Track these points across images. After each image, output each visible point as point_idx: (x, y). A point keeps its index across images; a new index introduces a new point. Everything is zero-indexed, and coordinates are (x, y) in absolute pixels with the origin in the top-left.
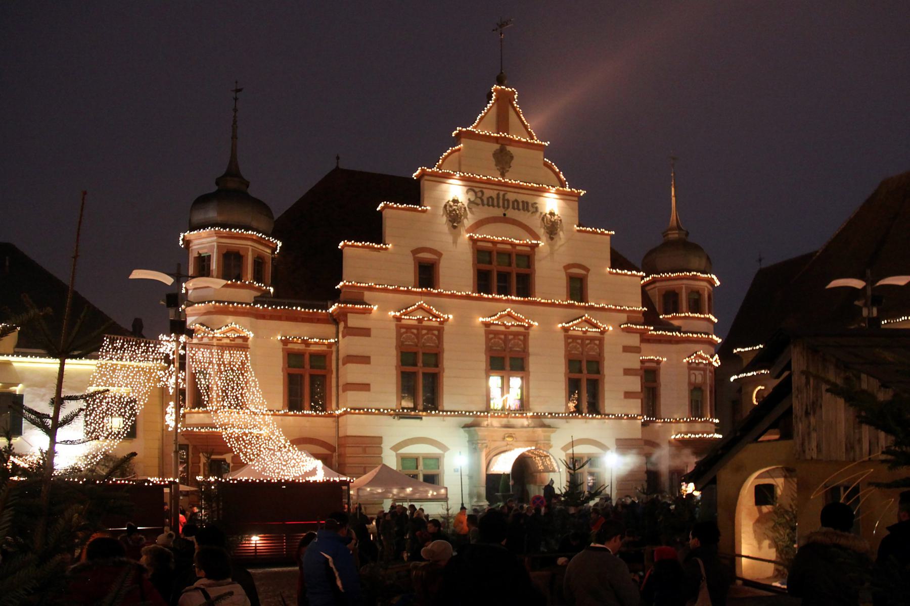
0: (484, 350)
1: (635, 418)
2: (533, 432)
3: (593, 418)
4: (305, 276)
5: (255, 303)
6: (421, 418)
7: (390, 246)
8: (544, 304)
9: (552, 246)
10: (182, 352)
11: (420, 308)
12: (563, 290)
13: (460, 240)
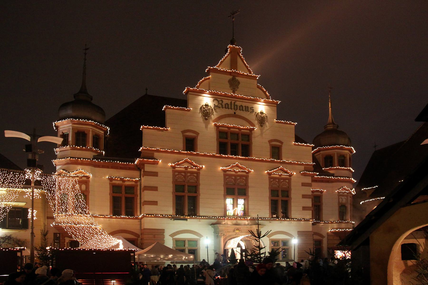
0: (223, 185)
1: (308, 220)
3: (284, 220)
4: (121, 144)
6: (187, 220)
8: (257, 161)
9: (262, 130)
11: (186, 161)
12: (268, 154)
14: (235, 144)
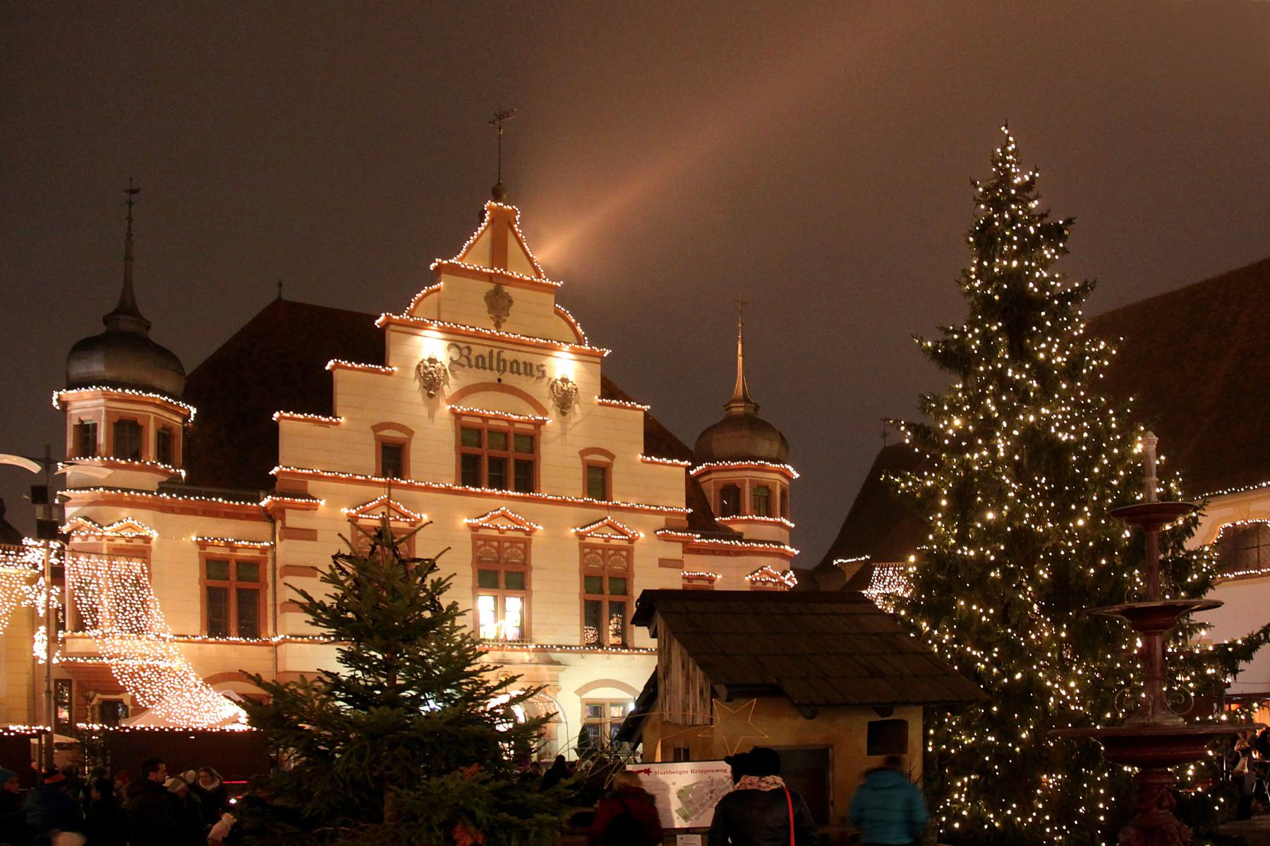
2: (536, 670)
4: (228, 458)
5: (160, 491)
7: (342, 420)
9: (564, 425)
10: (55, 561)
13: (438, 414)
14: (498, 459)
